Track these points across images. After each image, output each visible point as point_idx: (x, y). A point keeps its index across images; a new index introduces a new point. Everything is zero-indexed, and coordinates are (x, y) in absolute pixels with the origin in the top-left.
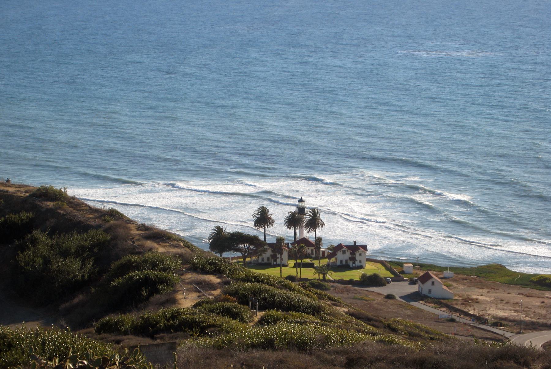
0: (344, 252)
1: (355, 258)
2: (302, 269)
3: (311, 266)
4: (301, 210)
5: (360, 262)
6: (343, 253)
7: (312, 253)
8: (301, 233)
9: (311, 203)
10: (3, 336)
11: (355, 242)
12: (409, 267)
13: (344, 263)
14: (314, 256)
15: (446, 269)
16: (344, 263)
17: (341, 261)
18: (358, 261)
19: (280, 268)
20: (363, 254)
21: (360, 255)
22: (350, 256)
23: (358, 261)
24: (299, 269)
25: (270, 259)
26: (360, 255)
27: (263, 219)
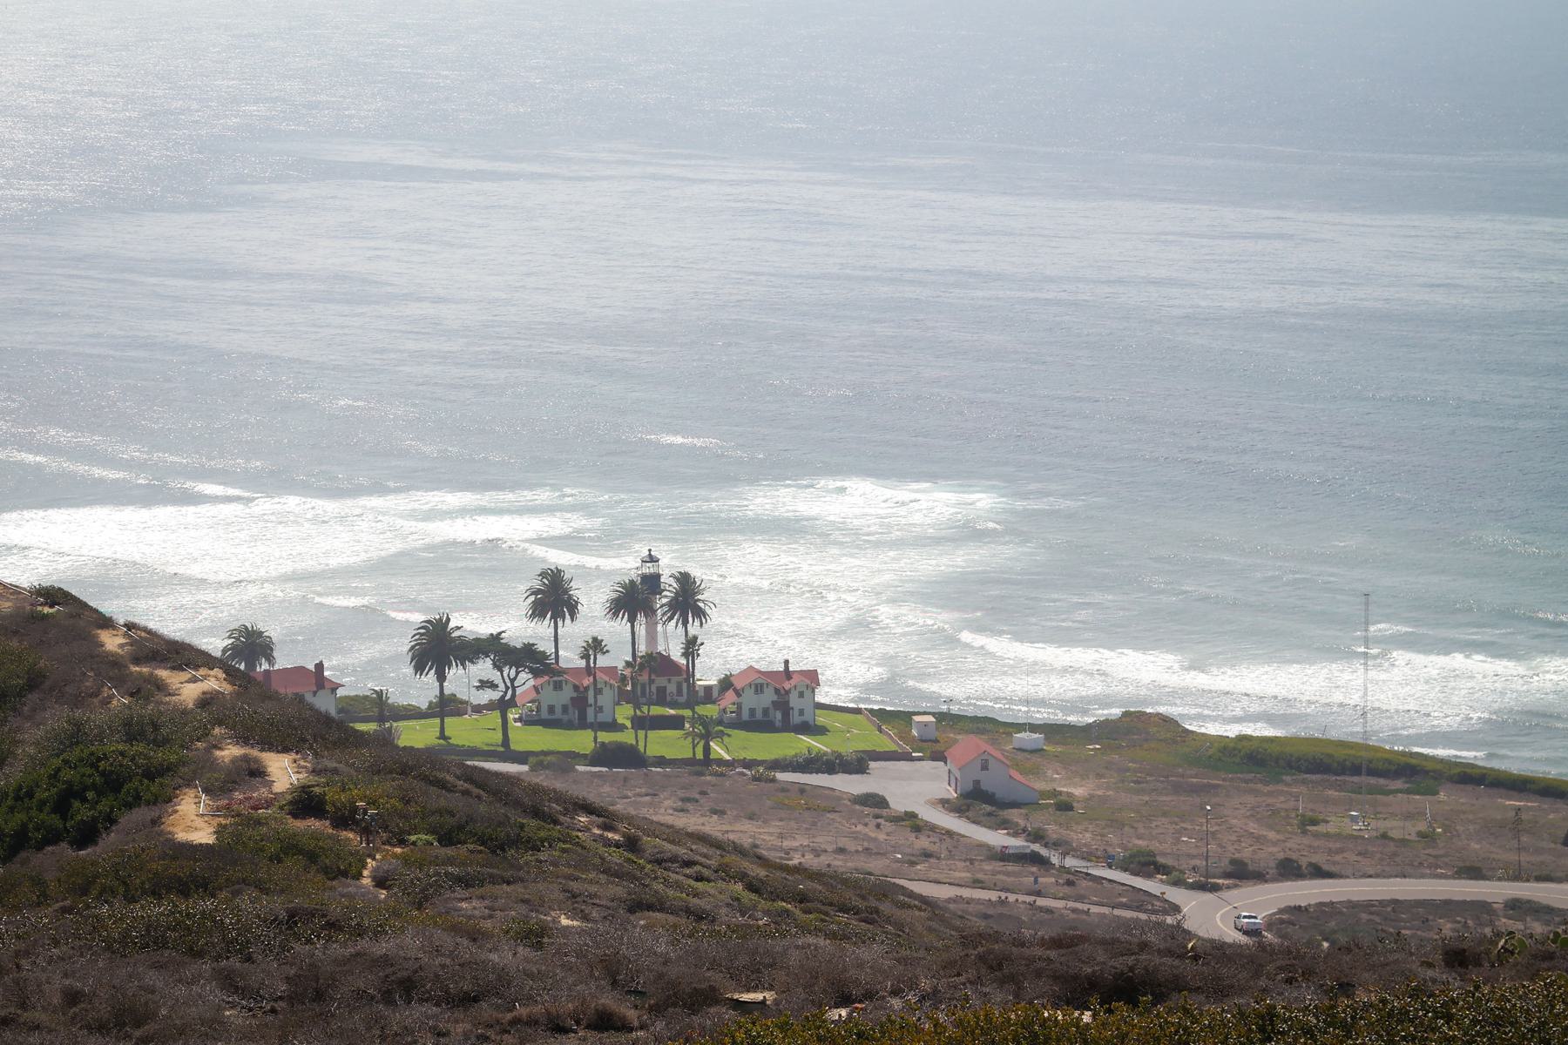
2: (651, 734)
3: (675, 723)
4: (652, 582)
5: (801, 712)
6: (555, 688)
7: (680, 692)
8: (652, 637)
9: (669, 565)
10: (32, 646)
11: (787, 662)
12: (926, 724)
13: (759, 715)
14: (682, 699)
15: (1020, 727)
16: (759, 715)
18: (796, 712)
19: (437, 721)
20: (807, 693)
22: (775, 698)
23: (796, 712)
24: (641, 733)
25: (771, 711)
26: (801, 695)
27: (554, 598)
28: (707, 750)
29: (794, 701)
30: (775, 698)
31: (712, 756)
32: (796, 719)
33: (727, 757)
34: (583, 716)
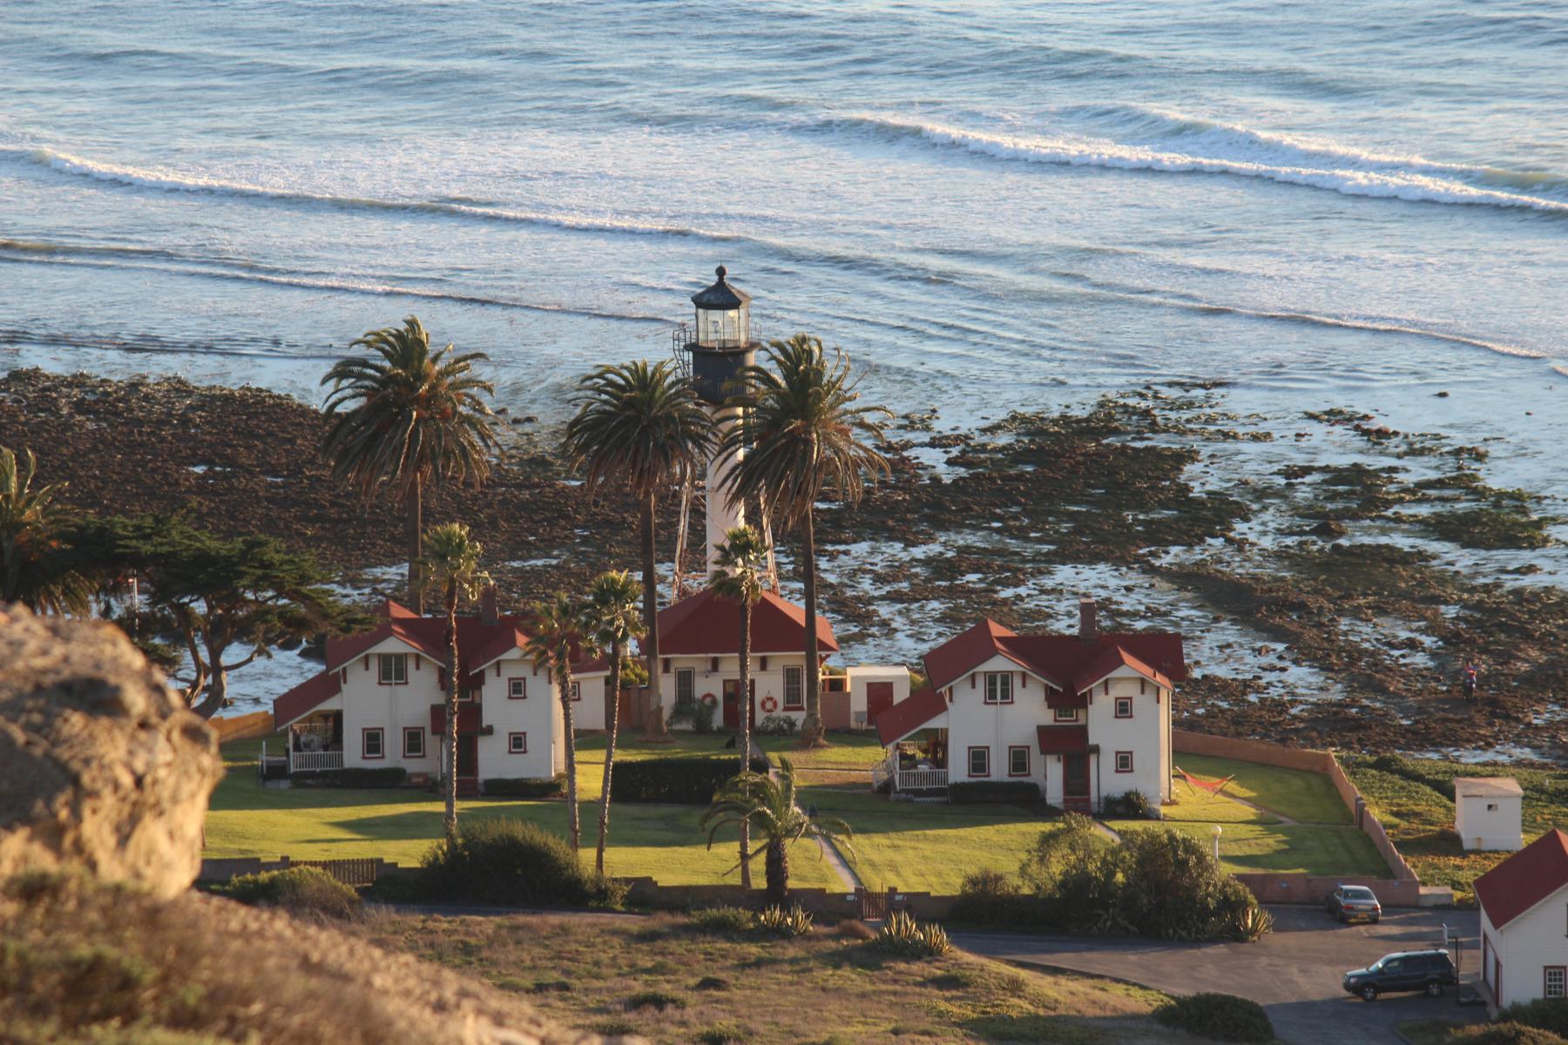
1: (1083, 730)
5: (1124, 762)
11: (721, 272)
13: (999, 770)
16: (999, 770)
17: (978, 758)
30: (1047, 717)
31: (792, 884)
32: (1107, 781)
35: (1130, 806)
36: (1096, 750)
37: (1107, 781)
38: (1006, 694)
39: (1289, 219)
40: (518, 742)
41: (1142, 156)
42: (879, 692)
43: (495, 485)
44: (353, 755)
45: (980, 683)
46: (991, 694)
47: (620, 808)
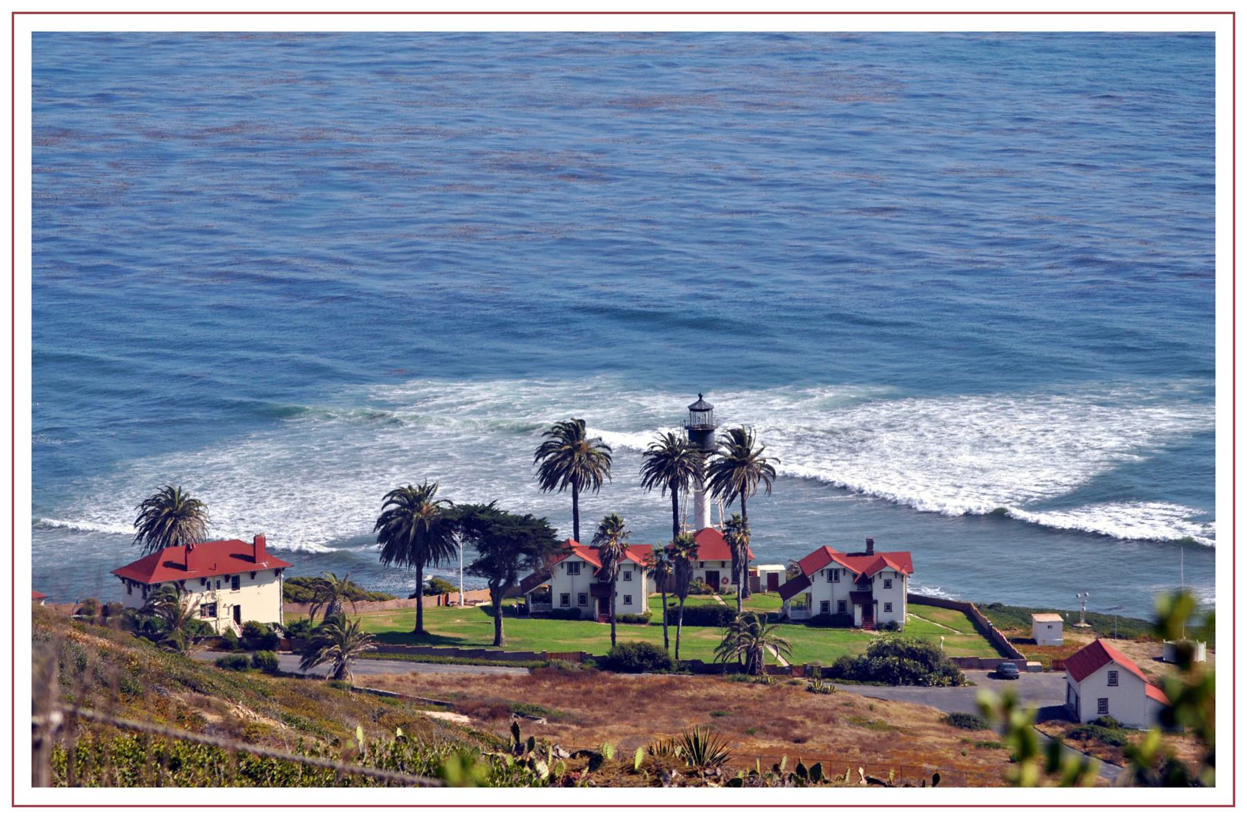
0: (574, 568)
1: (870, 593)
5: (888, 607)
11: (870, 543)
13: (834, 609)
16: (574, 602)
17: (825, 605)
20: (895, 582)
21: (888, 584)
24: (672, 629)
26: (888, 584)
28: (753, 653)
29: (879, 592)
30: (855, 589)
33: (785, 664)
34: (868, 613)
35: (892, 627)
36: (876, 602)
37: (880, 615)
38: (836, 578)
39: (898, 717)
40: (628, 600)
41: (1048, 517)
42: (773, 577)
43: (686, 547)
44: (556, 603)
45: (825, 574)
46: (830, 579)
47: (468, 578)
